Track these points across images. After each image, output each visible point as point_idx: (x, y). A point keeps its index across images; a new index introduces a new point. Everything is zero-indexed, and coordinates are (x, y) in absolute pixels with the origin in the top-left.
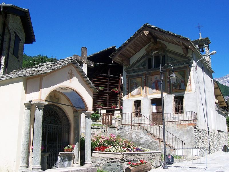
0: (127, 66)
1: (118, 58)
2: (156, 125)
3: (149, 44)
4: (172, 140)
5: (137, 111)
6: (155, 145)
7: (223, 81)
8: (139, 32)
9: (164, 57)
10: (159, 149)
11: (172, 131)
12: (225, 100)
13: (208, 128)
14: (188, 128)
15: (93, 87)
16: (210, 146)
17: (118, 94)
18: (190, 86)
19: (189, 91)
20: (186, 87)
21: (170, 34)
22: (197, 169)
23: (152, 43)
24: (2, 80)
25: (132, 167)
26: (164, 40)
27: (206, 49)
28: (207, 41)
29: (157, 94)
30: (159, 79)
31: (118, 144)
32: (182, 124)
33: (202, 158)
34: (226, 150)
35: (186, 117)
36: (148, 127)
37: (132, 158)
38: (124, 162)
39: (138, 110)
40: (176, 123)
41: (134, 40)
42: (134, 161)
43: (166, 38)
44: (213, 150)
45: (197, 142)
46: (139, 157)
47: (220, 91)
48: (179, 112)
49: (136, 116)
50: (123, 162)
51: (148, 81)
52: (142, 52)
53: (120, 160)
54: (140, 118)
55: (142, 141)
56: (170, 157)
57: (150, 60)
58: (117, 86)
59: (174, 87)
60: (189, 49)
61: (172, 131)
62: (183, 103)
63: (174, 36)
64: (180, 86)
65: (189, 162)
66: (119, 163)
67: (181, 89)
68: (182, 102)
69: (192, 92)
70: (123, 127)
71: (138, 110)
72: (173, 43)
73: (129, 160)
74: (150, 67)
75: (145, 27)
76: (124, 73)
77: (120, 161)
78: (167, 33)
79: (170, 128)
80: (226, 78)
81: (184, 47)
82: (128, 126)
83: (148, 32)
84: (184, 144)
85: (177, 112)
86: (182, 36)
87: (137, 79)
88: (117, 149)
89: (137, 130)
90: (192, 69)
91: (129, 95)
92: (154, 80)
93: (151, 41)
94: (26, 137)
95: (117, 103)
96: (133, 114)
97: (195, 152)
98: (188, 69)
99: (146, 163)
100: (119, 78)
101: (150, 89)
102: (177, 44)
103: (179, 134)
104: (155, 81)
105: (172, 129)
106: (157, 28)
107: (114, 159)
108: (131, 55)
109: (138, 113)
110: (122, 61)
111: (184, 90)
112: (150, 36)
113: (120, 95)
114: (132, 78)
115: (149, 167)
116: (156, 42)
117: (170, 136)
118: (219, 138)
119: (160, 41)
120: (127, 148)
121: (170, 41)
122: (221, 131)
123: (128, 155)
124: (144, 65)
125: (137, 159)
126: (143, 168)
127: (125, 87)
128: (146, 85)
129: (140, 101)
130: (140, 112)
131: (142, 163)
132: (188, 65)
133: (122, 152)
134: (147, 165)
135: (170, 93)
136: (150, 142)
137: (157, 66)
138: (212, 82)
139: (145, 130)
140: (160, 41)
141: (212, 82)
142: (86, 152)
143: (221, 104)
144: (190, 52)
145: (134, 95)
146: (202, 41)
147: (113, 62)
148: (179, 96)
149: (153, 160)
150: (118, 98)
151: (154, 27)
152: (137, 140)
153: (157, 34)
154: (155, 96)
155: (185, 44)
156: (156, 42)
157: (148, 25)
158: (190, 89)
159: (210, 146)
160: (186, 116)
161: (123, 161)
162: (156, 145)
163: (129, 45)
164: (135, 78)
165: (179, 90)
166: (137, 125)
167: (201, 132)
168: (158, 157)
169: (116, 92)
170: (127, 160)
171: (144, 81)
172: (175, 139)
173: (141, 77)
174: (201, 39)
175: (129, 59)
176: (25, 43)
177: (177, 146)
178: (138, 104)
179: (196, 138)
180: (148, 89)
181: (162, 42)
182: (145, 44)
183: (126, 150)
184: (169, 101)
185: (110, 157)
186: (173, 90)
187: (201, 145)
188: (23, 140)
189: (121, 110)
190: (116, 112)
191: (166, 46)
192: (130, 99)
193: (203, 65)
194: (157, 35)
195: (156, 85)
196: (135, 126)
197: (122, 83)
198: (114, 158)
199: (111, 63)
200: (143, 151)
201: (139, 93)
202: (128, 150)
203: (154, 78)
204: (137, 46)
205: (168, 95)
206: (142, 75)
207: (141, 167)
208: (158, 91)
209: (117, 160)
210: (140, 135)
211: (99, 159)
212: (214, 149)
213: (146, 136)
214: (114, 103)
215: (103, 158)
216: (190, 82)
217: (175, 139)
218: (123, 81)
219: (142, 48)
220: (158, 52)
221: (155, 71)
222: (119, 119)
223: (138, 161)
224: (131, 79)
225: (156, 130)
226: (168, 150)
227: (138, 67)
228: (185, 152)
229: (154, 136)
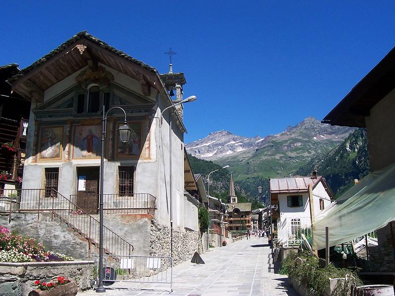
0: (38, 104)
1: (23, 85)
2: (85, 214)
3: (83, 69)
4: (111, 242)
5: (50, 188)
7: (191, 150)
8: (69, 45)
9: (107, 95)
10: (87, 256)
11: (112, 226)
13: (171, 223)
14: (141, 222)
16: (172, 253)
17: (13, 153)
18: (147, 150)
19: (146, 159)
20: (141, 152)
21: (123, 57)
22: (156, 292)
23: (90, 67)
25: (42, 289)
26: (110, 66)
27: (178, 91)
28: (180, 79)
29: (92, 161)
30: (94, 132)
31: (15, 245)
32: (129, 215)
33: (170, 269)
34: (198, 260)
37: (42, 272)
38: (27, 281)
39: (52, 186)
40: (119, 213)
41: (56, 58)
42: (45, 278)
43: (115, 61)
45: (153, 246)
46: (55, 271)
47: (189, 164)
48: (125, 193)
49: (47, 197)
50: (24, 282)
52: (69, 82)
53: (20, 276)
54: (56, 200)
55: (56, 242)
56: (109, 272)
57: (81, 98)
58: (14, 138)
59: (120, 150)
60: (151, 88)
61: (112, 226)
62: (133, 179)
63: (130, 60)
64: (131, 149)
65: (137, 280)
66: (17, 284)
67: (132, 154)
68: (131, 177)
69: (150, 161)
70: (23, 216)
71: (52, 186)
72: (126, 73)
73: (35, 277)
74: (80, 109)
75: (81, 38)
76: (32, 116)
77: (19, 279)
78: (118, 55)
79: (108, 221)
80: (197, 145)
82: (31, 213)
83: (86, 47)
84: (131, 250)
85: (122, 193)
86: (144, 63)
87: (55, 129)
88: (13, 255)
90: (154, 121)
91: (36, 158)
92: (85, 134)
93: (87, 64)
95: (10, 171)
96: (43, 192)
97: (153, 263)
98: (148, 121)
99: (69, 281)
100: (19, 125)
101: (77, 150)
102: (133, 77)
103: (124, 232)
104: (88, 136)
105: (112, 222)
106: (101, 42)
107: (8, 275)
108: (49, 84)
109: (51, 190)
110: (31, 93)
111: (137, 157)
112: (87, 56)
113: (17, 155)
114: (45, 126)
115: (73, 290)
116: (96, 68)
119: (104, 66)
120: (32, 255)
121: (121, 68)
122: (190, 230)
123: (34, 267)
124: (70, 105)
125: (50, 275)
126: (63, 292)
127: (32, 140)
128: (70, 142)
129: (56, 170)
130: (56, 188)
131: (61, 282)
132: (147, 113)
133: (23, 261)
134: (71, 286)
135: (112, 159)
136: (72, 245)
137: (95, 108)
139: (63, 221)
140: (104, 66)
143: (189, 186)
144: (153, 90)
145: (46, 158)
146: (174, 77)
147: (12, 92)
148: (128, 166)
149: (79, 276)
150: (13, 162)
151: (97, 39)
152: (48, 240)
153: (100, 53)
154: (92, 163)
155: (148, 77)
156: (96, 68)
157: (87, 34)
158: (147, 156)
159: (172, 253)
160: (137, 201)
161: (25, 279)
162: (83, 251)
163: (46, 65)
164: (52, 127)
166: (48, 211)
168: (88, 271)
169: (10, 149)
171: (68, 134)
172: (117, 240)
173: (63, 127)
174: (171, 75)
175: (43, 91)
177: (119, 252)
178: (52, 174)
179: (152, 240)
180: (73, 149)
181: (108, 69)
182: (77, 68)
183: (30, 257)
184: (111, 172)
187: (159, 252)
189: (19, 186)
190: (7, 186)
191: (113, 77)
193: (171, 117)
194: (100, 54)
195: (89, 143)
196: (45, 215)
197: (24, 134)
198: (7, 273)
199: (9, 94)
200: (62, 259)
202: (33, 257)
203: (86, 131)
204: (62, 69)
205: (109, 162)
206: (65, 122)
207: (60, 289)
208: (90, 154)
209: (13, 277)
210: (53, 231)
213: (65, 233)
214: (6, 170)
216: (149, 144)
217: (117, 240)
218: (25, 130)
219: (69, 74)
220: (97, 85)
221: (88, 118)
222: (15, 201)
224: (75, 126)
225: (85, 223)
227: (59, 107)
228: (135, 263)
229: (80, 234)
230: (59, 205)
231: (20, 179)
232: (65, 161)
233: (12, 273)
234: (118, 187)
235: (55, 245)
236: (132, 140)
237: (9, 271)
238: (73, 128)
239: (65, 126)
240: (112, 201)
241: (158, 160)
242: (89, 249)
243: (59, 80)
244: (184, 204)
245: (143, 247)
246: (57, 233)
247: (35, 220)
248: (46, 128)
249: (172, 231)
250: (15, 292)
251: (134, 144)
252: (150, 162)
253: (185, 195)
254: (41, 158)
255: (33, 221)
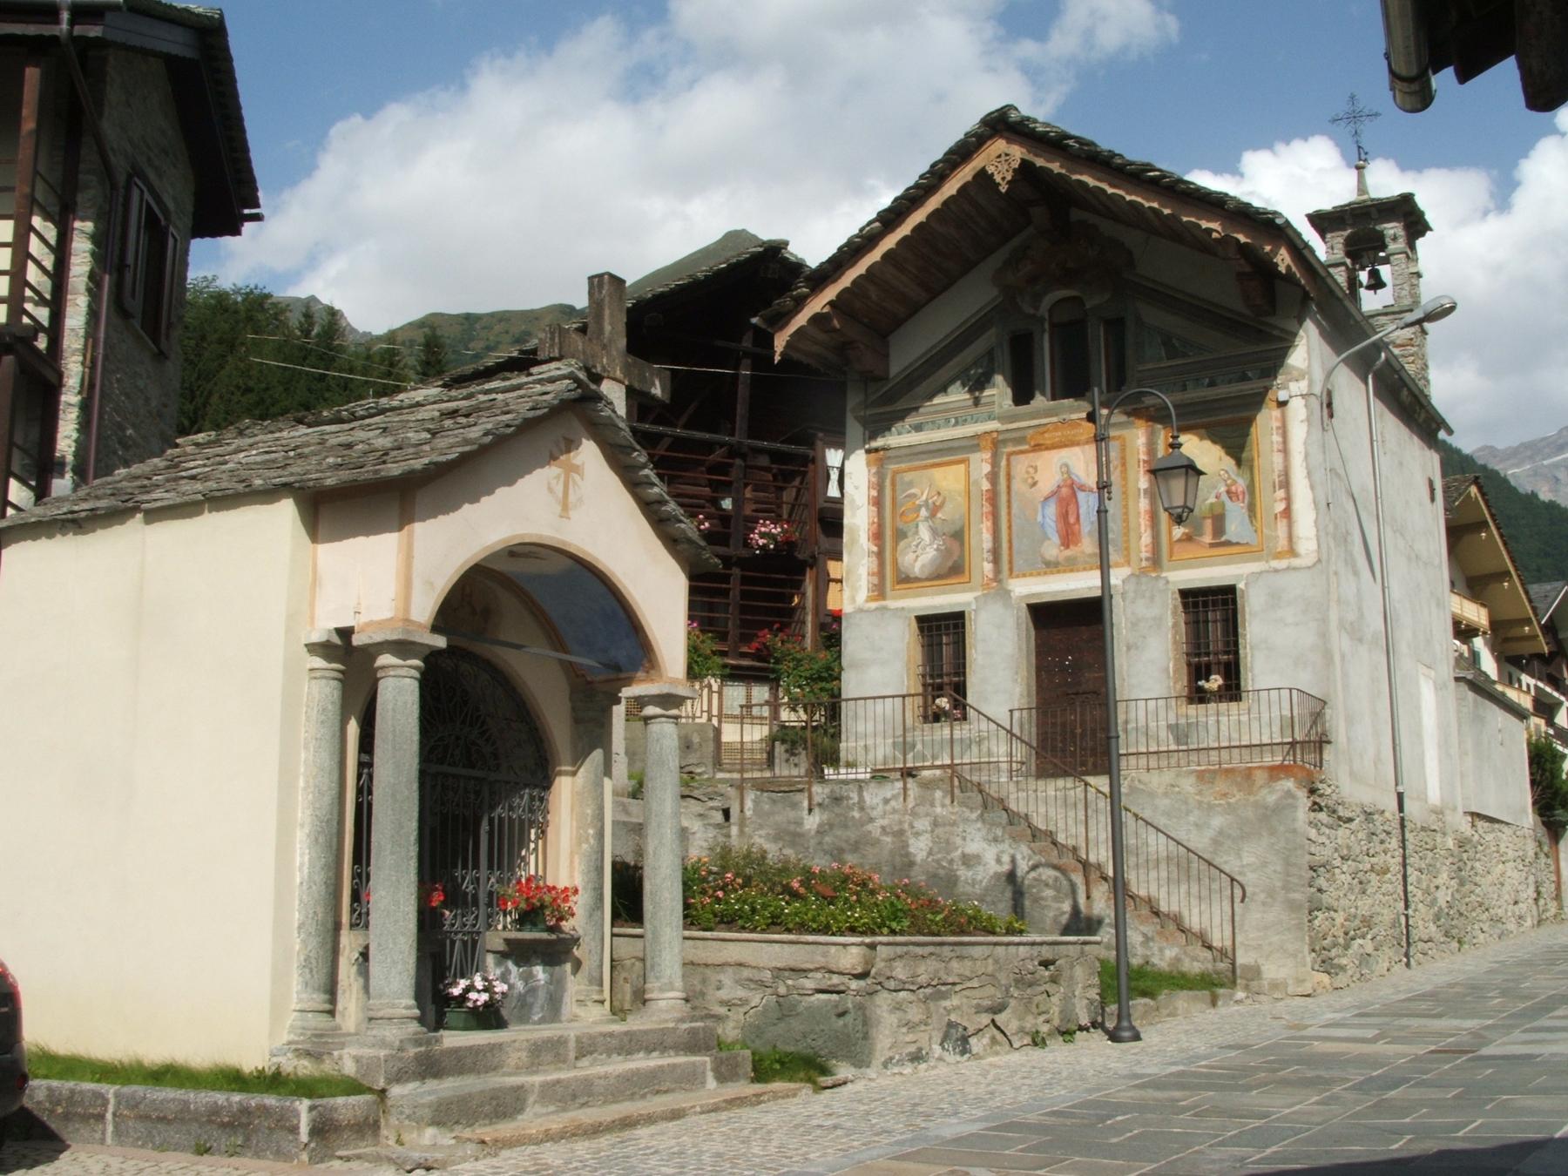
3: (1016, 242)
4: (1164, 874)
6: (1056, 905)
7: (1535, 473)
12: (1534, 609)
13: (1400, 796)
15: (690, 541)
16: (1410, 912)
18: (1282, 526)
24: (159, 504)
32: (1227, 771)
35: (1255, 725)
36: (1012, 787)
44: (1430, 940)
45: (1321, 882)
51: (1009, 487)
54: (961, 731)
61: (1167, 814)
67: (1228, 543)
69: (1296, 562)
79: (1152, 795)
81: (1248, 269)
84: (1237, 900)
87: (937, 473)
89: (939, 810)
94: (321, 840)
103: (1210, 833)
105: (1167, 801)
107: (819, 975)
114: (903, 466)
117: (1152, 849)
118: (1477, 865)
125: (950, 980)
138: (1432, 490)
139: (991, 804)
141: (1432, 490)
142: (653, 934)
145: (917, 580)
158: (1282, 543)
164: (926, 467)
165: (1212, 545)
166: (938, 772)
167: (1350, 820)
170: (892, 984)
171: (986, 485)
176: (194, 236)
185: (792, 964)
186: (1176, 548)
188: (302, 855)
192: (891, 604)
196: (928, 785)
198: (817, 970)
201: (950, 564)
206: (973, 444)
209: (836, 979)
210: (958, 841)
211: (727, 978)
212: (1439, 937)
215: (746, 973)
223: (958, 988)
224: (895, 473)
226: (1141, 939)
230: (975, 748)
231: (97, 270)
232: (985, 586)
233: (833, 967)
234: (1185, 670)
235: (969, 889)
236: (1223, 489)
237: (820, 960)
238: (1003, 463)
239: (975, 457)
240: (1163, 723)
241: (1324, 557)
242: (1088, 897)
243: (933, 293)
244: (1459, 719)
245: (1284, 888)
246: (973, 847)
247: (893, 803)
248: (910, 470)
249: (1403, 826)
250: (845, 1025)
251: (1229, 505)
252: (1295, 569)
253: (1457, 679)
254: (898, 583)
255: (888, 808)
